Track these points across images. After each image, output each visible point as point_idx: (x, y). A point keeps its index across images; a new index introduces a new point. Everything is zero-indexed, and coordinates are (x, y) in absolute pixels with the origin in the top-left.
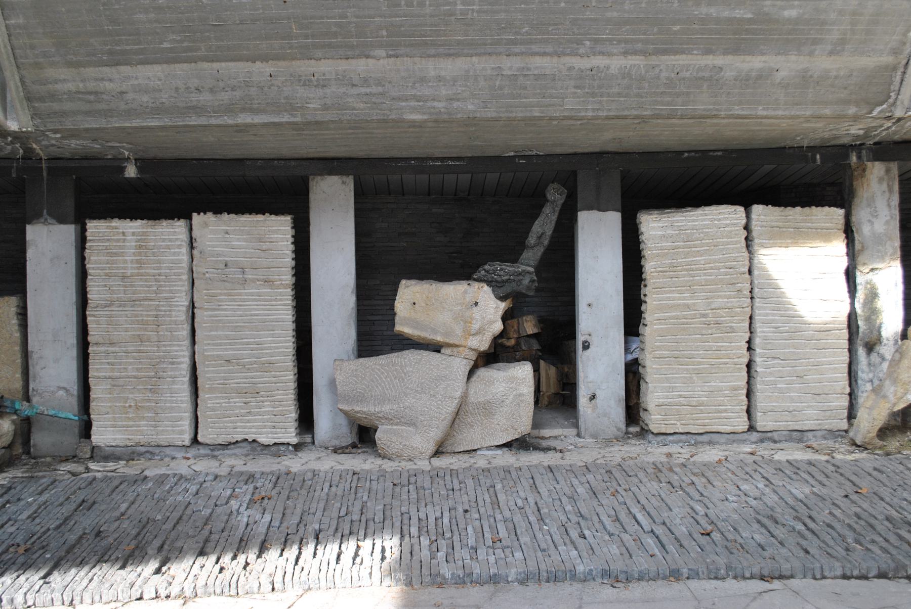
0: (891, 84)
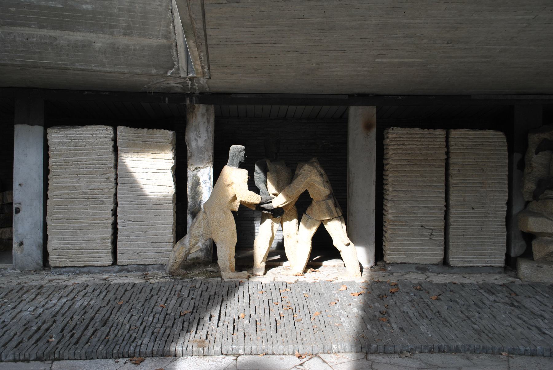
0: (172, 57)
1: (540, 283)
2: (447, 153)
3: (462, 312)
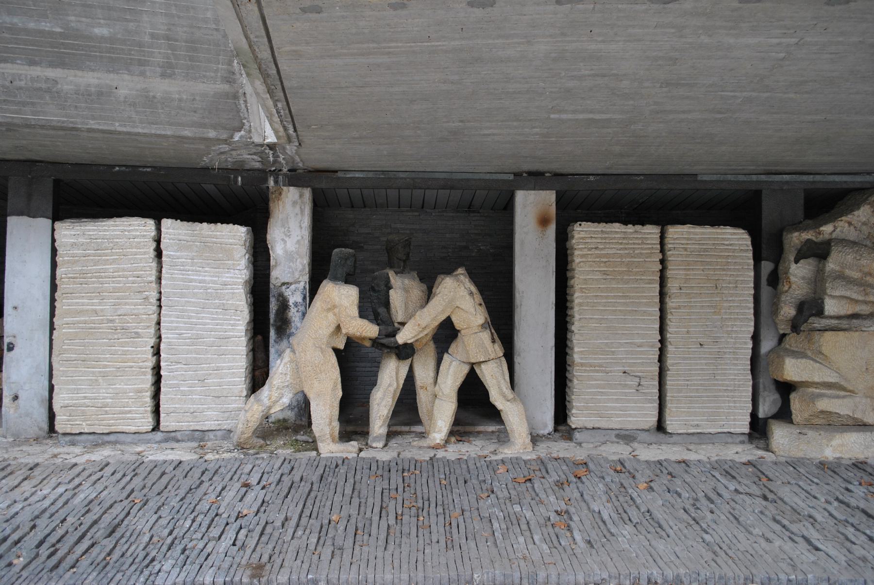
0: (238, 111)
1: (802, 458)
2: (662, 262)
3: (685, 511)
